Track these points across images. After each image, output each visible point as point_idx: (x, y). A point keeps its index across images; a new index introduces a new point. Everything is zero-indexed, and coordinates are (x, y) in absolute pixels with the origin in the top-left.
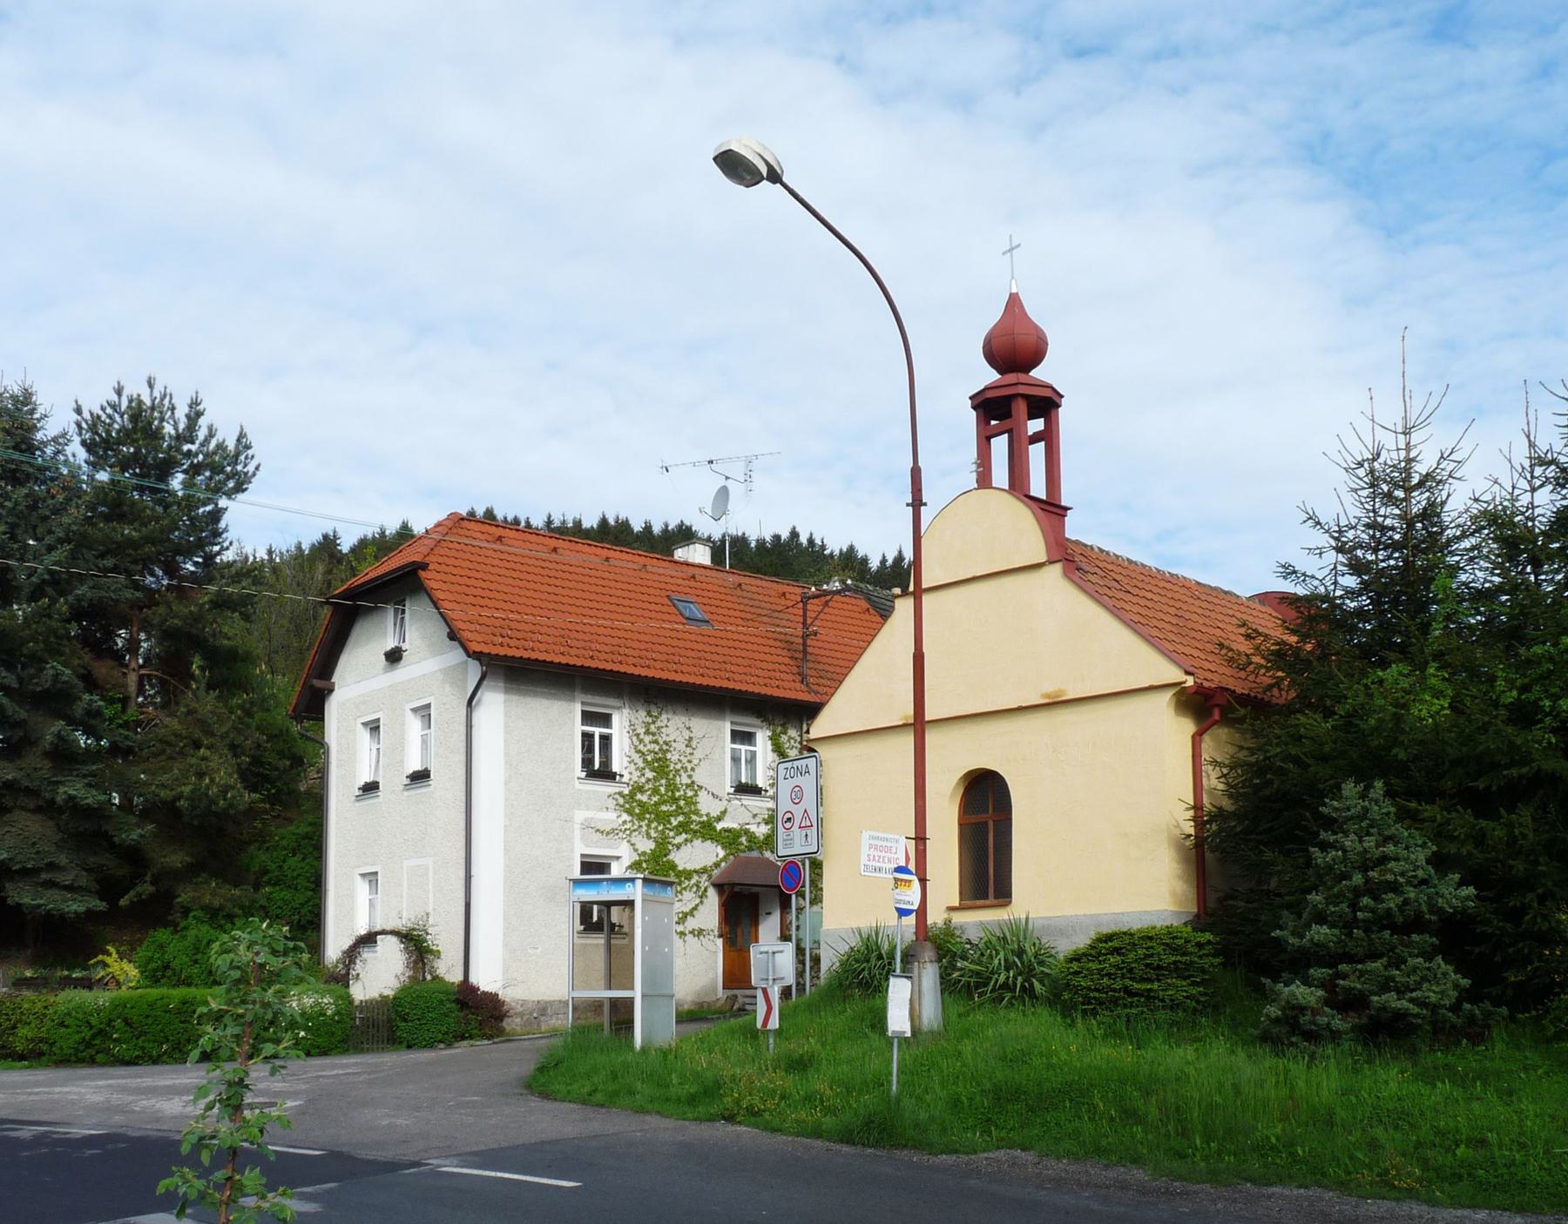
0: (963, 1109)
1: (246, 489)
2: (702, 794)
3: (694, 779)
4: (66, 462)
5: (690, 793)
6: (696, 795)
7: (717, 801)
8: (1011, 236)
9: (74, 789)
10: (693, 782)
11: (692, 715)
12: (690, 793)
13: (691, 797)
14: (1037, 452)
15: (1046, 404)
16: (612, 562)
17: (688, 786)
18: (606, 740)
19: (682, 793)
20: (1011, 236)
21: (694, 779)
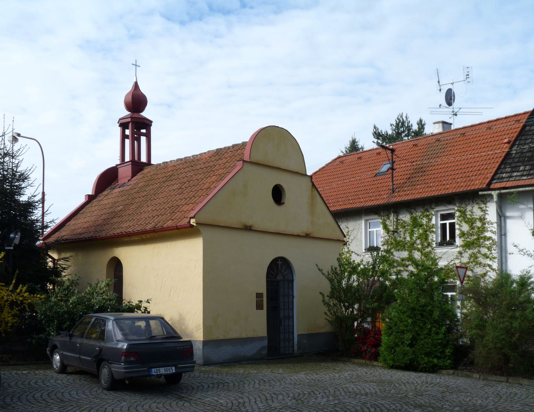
0: (422, 332)
1: (412, 125)
2: (353, 255)
3: (350, 249)
4: (482, 289)
5: (348, 255)
6: (351, 256)
7: (359, 256)
8: (136, 60)
9: (287, 392)
10: (349, 250)
11: (349, 221)
12: (348, 255)
13: (349, 257)
14: (143, 139)
15: (147, 124)
16: (344, 162)
17: (347, 252)
18: (452, 225)
19: (345, 256)
20: (136, 60)
21: (350, 249)
